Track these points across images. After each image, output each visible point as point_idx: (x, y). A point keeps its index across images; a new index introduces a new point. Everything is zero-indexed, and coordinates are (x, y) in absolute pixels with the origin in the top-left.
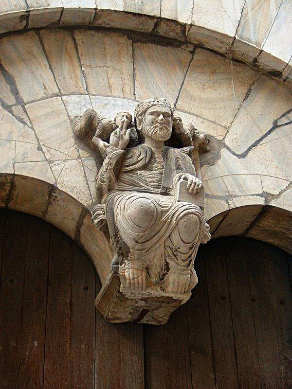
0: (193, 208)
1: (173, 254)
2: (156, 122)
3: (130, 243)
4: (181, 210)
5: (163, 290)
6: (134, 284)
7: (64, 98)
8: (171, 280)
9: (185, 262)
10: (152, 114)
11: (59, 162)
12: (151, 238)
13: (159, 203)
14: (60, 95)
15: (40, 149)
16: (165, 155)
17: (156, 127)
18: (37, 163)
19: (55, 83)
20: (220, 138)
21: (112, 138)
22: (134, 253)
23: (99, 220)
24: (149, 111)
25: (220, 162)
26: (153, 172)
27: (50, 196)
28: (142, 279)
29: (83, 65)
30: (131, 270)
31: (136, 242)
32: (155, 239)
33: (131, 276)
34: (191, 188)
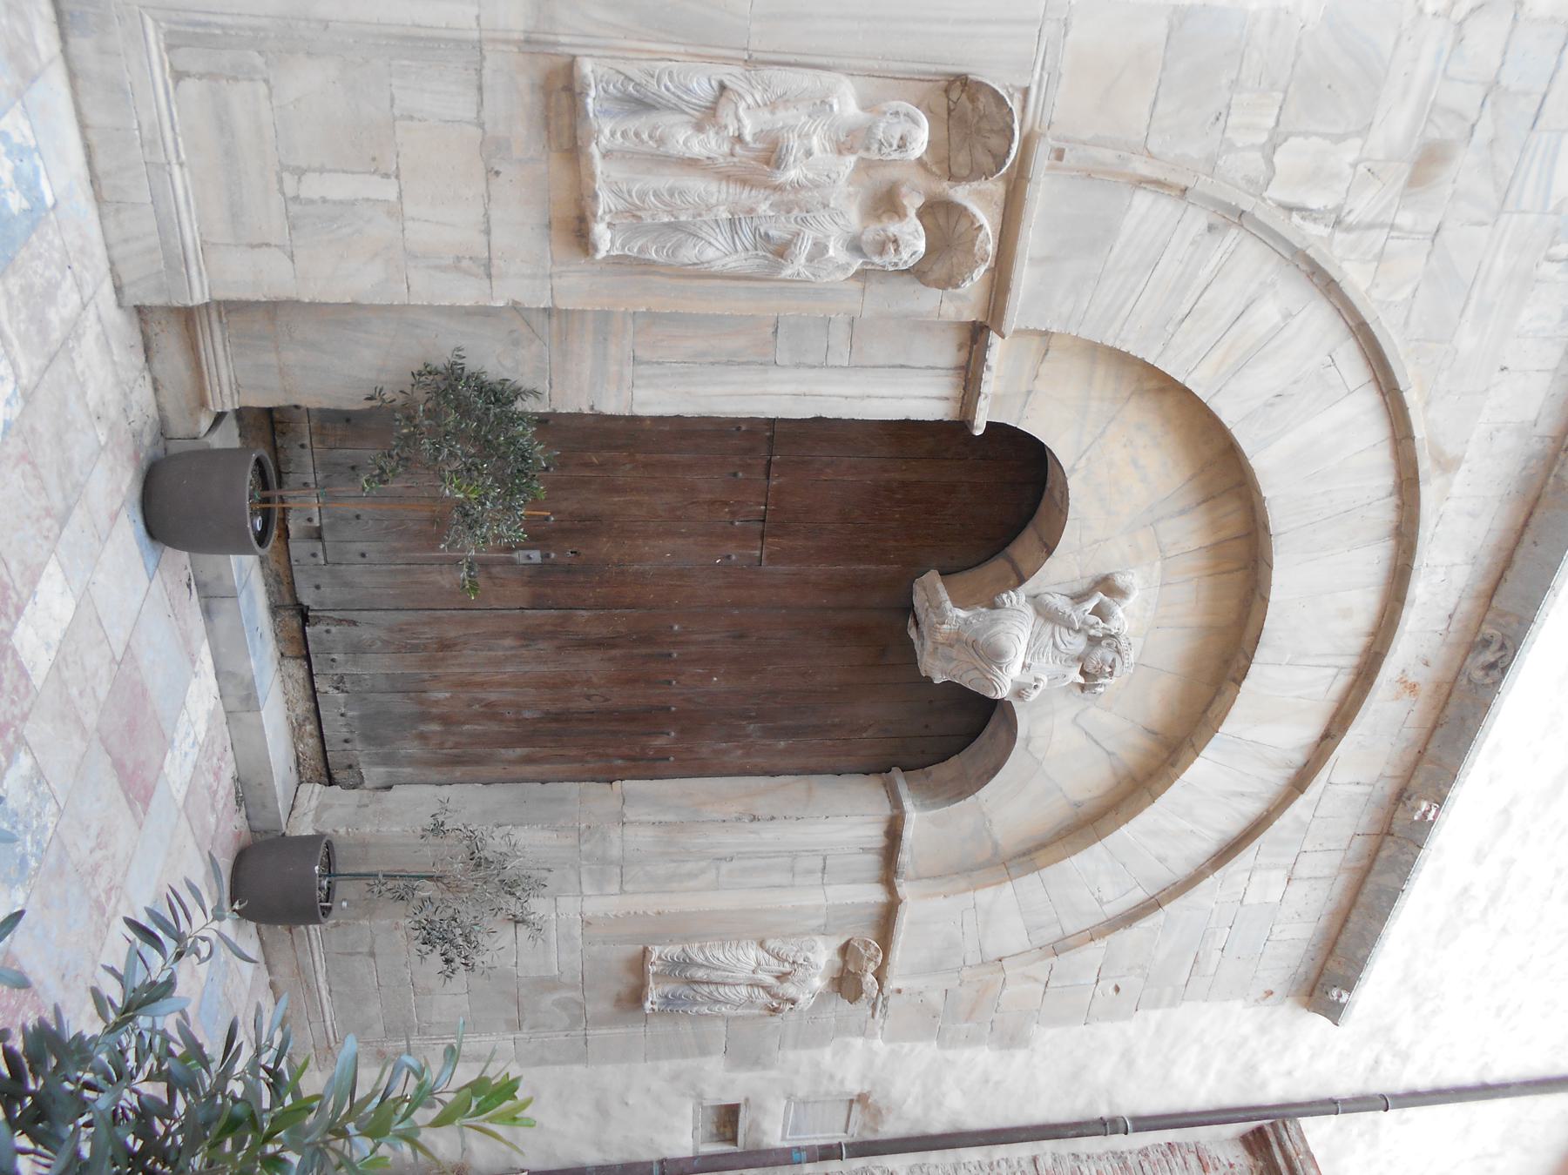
21: (1094, 619)
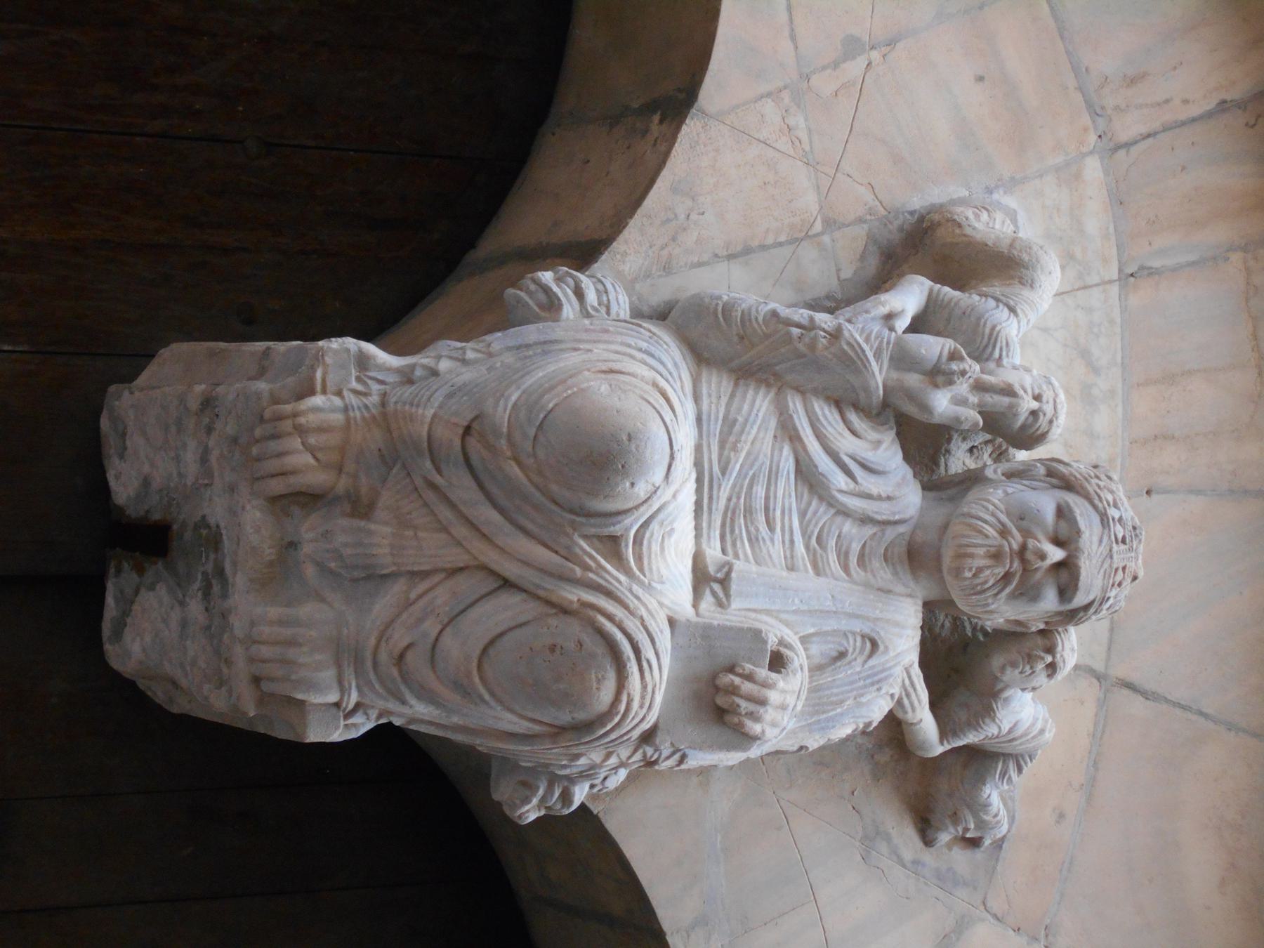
0: (644, 687)
4: (632, 625)
13: (654, 526)
15: (852, 47)
18: (786, 33)
21: (932, 346)
24: (1071, 499)
27: (650, 108)
33: (311, 417)
34: (737, 680)
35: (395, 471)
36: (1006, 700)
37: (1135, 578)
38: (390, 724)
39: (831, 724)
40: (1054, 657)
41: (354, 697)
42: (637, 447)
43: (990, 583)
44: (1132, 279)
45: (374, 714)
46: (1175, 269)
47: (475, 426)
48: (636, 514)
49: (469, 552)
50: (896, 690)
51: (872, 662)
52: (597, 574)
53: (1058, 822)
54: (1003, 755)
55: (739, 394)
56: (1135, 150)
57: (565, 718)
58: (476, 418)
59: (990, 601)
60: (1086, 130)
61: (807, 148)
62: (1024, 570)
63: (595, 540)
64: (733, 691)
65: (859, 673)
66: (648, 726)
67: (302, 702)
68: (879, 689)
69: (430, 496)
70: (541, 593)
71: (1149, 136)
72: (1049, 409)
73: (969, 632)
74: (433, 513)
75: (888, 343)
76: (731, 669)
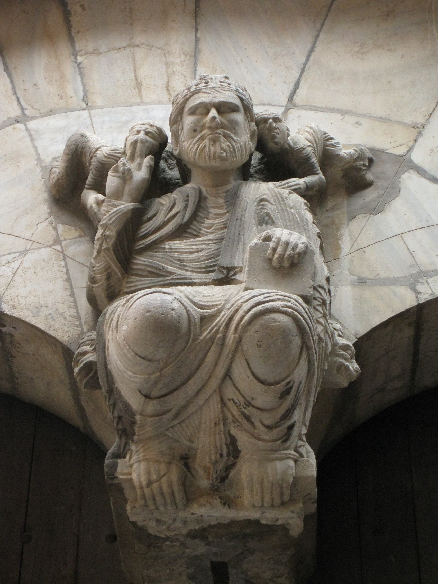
0: (279, 300)
1: (243, 414)
2: (203, 127)
3: (134, 401)
4: (246, 307)
5: (228, 502)
6: (153, 497)
7: (32, 125)
8: (244, 477)
9: (276, 431)
10: (193, 112)
11: (10, 257)
12: (183, 384)
13: (196, 300)
14: (23, 119)
16: (232, 199)
17: (202, 139)
19: (14, 98)
20: (400, 151)
21: (112, 181)
22: (145, 428)
23: (81, 365)
24: (187, 109)
25: (398, 204)
26: (200, 239)
28: (170, 485)
29: (80, 51)
30: (143, 466)
31: (147, 397)
32: (193, 385)
35: (169, 434)
36: (295, 143)
37: (226, 78)
38: (306, 435)
39: (305, 220)
40: (270, 118)
41: (292, 452)
42: (153, 308)
43: (229, 144)
44: (89, 104)
45: (300, 443)
46: (84, 85)
47: (144, 392)
48: (189, 308)
49: (212, 394)
50: (287, 191)
51: (272, 201)
52: (220, 326)
53: (360, 125)
54: (324, 147)
55: (135, 272)
56: (25, 106)
57: (297, 341)
58: (139, 391)
59: (239, 145)
60: (14, 128)
61: (18, 254)
62: (222, 128)
63: (203, 329)
64: (281, 257)
65: (277, 206)
66: (301, 299)
67: (294, 478)
68: (286, 198)
69: (184, 416)
70: (231, 355)
71: (18, 101)
72: (144, 127)
73: (262, 166)
74: (192, 414)
75: (110, 202)
76: (270, 260)
